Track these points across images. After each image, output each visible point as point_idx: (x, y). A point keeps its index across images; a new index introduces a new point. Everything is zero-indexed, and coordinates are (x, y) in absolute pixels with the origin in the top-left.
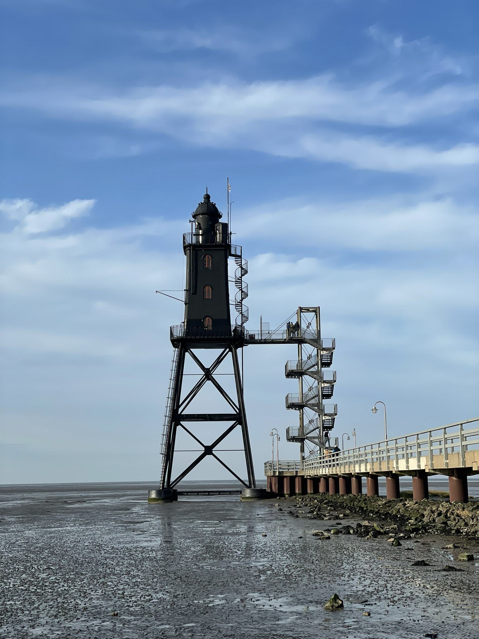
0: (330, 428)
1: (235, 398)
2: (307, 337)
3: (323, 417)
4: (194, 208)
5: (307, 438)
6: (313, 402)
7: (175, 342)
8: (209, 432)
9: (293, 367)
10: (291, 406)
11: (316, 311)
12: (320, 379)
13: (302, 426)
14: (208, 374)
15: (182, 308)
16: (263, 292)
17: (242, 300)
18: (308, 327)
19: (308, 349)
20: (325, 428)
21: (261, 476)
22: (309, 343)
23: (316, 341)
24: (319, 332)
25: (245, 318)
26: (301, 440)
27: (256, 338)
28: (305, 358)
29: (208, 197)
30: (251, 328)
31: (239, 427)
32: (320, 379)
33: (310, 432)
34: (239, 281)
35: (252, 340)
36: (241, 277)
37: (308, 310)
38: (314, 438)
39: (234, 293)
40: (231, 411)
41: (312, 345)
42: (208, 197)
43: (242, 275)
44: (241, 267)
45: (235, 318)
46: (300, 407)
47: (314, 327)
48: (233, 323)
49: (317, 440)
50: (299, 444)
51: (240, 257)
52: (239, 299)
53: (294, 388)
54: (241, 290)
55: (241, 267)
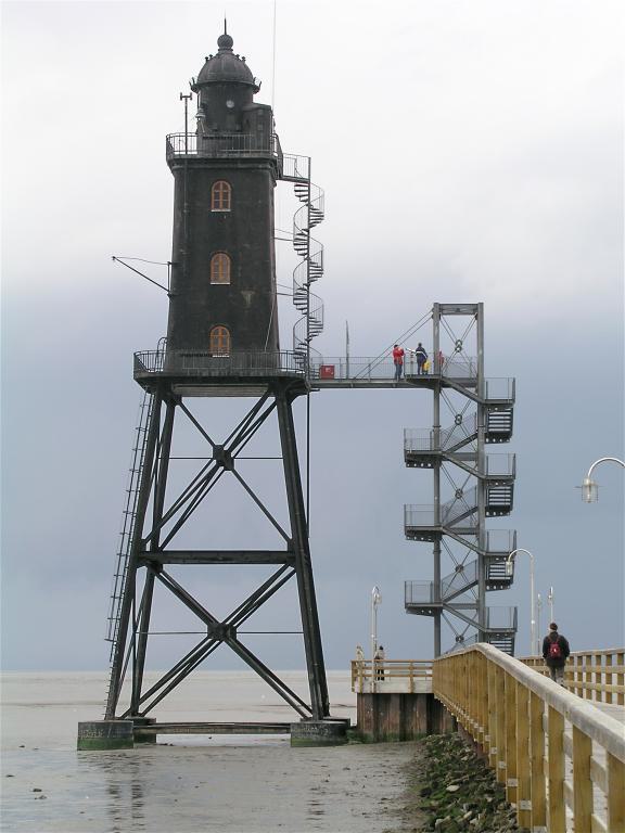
1: (305, 693)
2: (450, 373)
5: (452, 609)
6: (464, 524)
7: (147, 380)
8: (222, 591)
9: (423, 445)
10: (414, 533)
11: (476, 310)
13: (437, 585)
15: (163, 303)
21: (344, 702)
24: (481, 359)
25: (314, 327)
26: (434, 611)
27: (337, 376)
28: (447, 422)
29: (225, 42)
30: (324, 350)
31: (291, 588)
33: (448, 622)
34: (302, 240)
36: (308, 286)
37: (457, 309)
39: (287, 264)
40: (283, 546)
42: (225, 42)
43: (311, 226)
45: (288, 318)
46: (432, 535)
47: (470, 348)
48: (286, 342)
49: (472, 464)
50: (431, 545)
51: (307, 182)
52: (303, 337)
54: (308, 259)
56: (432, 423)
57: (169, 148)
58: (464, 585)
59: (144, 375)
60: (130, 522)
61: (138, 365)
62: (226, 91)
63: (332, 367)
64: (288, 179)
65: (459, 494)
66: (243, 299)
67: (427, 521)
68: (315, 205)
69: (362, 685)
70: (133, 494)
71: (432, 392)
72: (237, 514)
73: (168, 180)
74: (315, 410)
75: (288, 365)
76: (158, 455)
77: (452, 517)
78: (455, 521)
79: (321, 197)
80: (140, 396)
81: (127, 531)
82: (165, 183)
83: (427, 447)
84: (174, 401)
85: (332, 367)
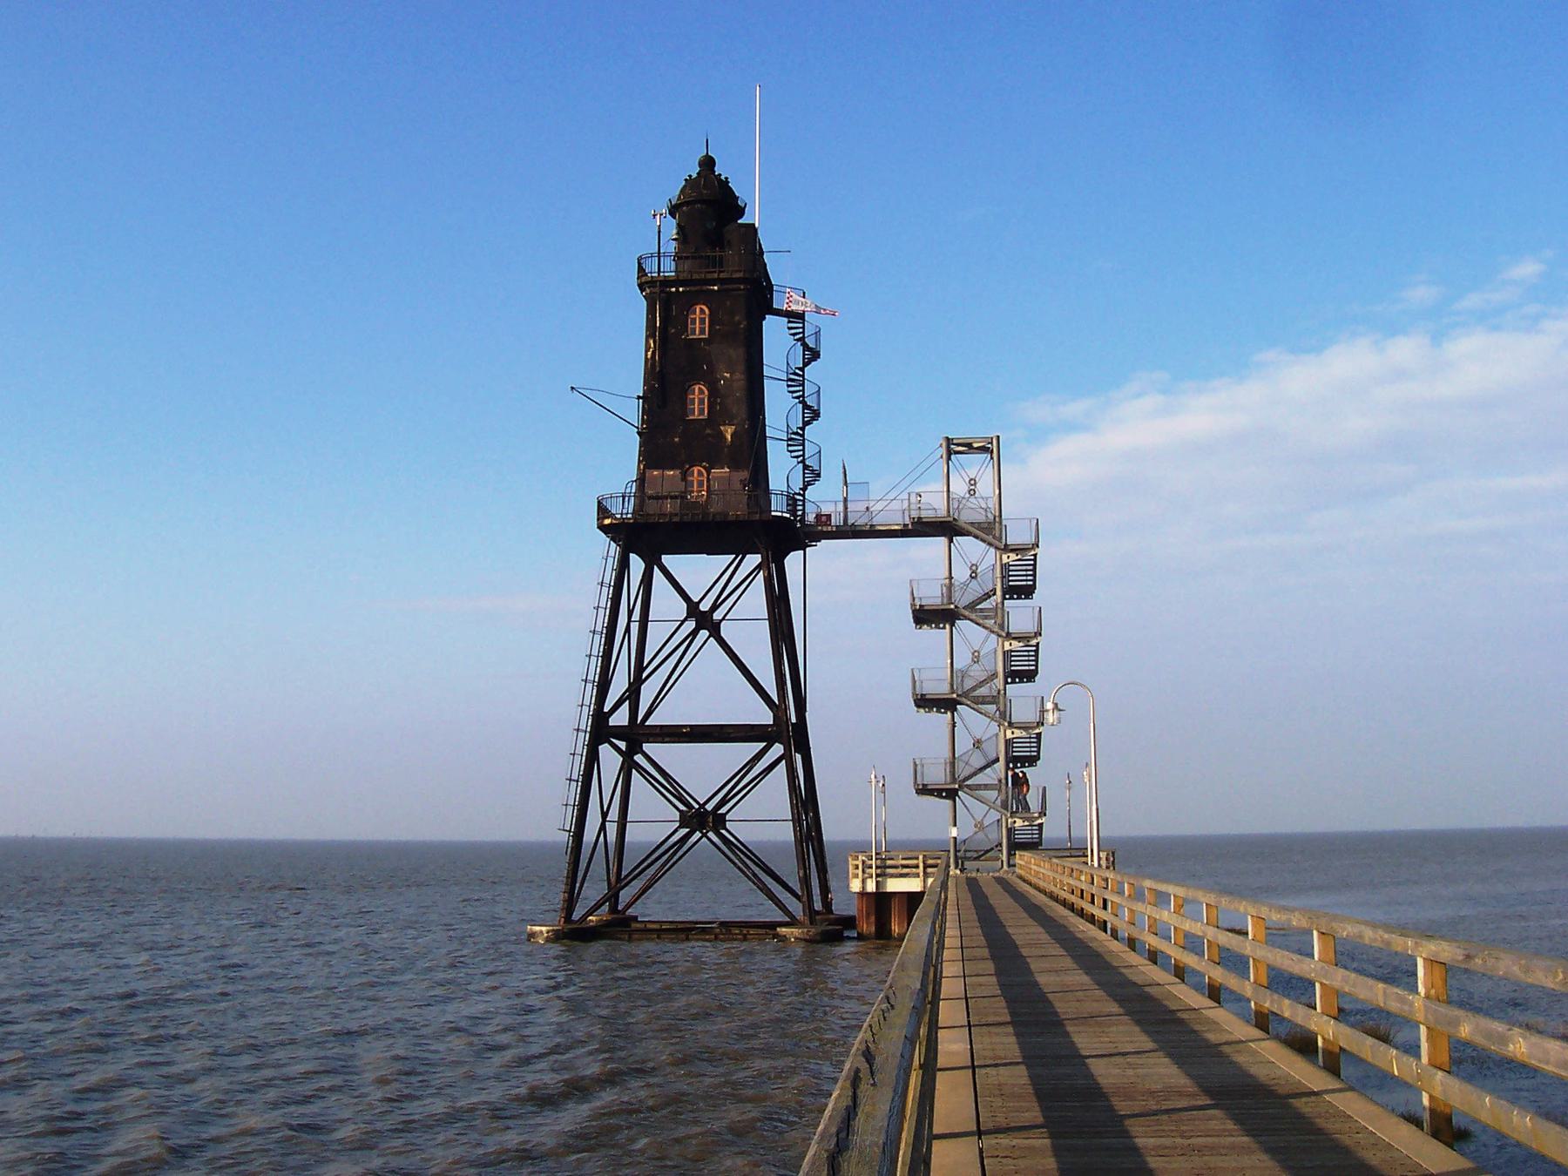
0: (1032, 760)
2: (965, 518)
3: (1009, 732)
4: (674, 191)
9: (932, 596)
12: (1004, 717)
14: (704, 620)
16: (853, 422)
17: (804, 489)
18: (972, 492)
19: (969, 548)
20: (1013, 760)
22: (976, 537)
23: (989, 531)
29: (708, 163)
30: (823, 499)
32: (1004, 717)
33: (974, 774)
34: (796, 380)
35: (822, 530)
36: (803, 429)
38: (986, 787)
39: (779, 407)
40: (765, 717)
41: (983, 541)
42: (708, 163)
43: (806, 424)
44: (804, 403)
45: (781, 470)
46: (947, 705)
47: (986, 487)
50: (949, 802)
52: (797, 486)
53: (932, 656)
54: (803, 462)
55: (804, 403)
56: (947, 754)
57: (641, 269)
58: (983, 763)
59: (607, 522)
60: (591, 692)
61: (603, 511)
62: (709, 211)
63: (829, 516)
64: (778, 313)
65: (976, 658)
66: (722, 436)
67: (940, 688)
68: (811, 343)
69: (864, 881)
70: (594, 659)
71: (939, 1074)
72: (708, 689)
73: (638, 305)
74: (816, 571)
75: (778, 508)
76: (630, 613)
77: (969, 684)
78: (974, 689)
79: (817, 334)
80: (604, 549)
81: (587, 702)
82: (635, 311)
83: (939, 601)
84: (652, 561)
85: (829, 516)
